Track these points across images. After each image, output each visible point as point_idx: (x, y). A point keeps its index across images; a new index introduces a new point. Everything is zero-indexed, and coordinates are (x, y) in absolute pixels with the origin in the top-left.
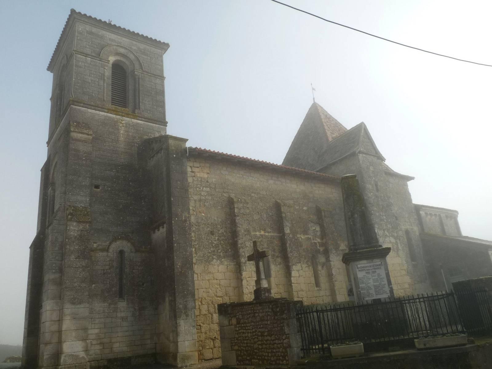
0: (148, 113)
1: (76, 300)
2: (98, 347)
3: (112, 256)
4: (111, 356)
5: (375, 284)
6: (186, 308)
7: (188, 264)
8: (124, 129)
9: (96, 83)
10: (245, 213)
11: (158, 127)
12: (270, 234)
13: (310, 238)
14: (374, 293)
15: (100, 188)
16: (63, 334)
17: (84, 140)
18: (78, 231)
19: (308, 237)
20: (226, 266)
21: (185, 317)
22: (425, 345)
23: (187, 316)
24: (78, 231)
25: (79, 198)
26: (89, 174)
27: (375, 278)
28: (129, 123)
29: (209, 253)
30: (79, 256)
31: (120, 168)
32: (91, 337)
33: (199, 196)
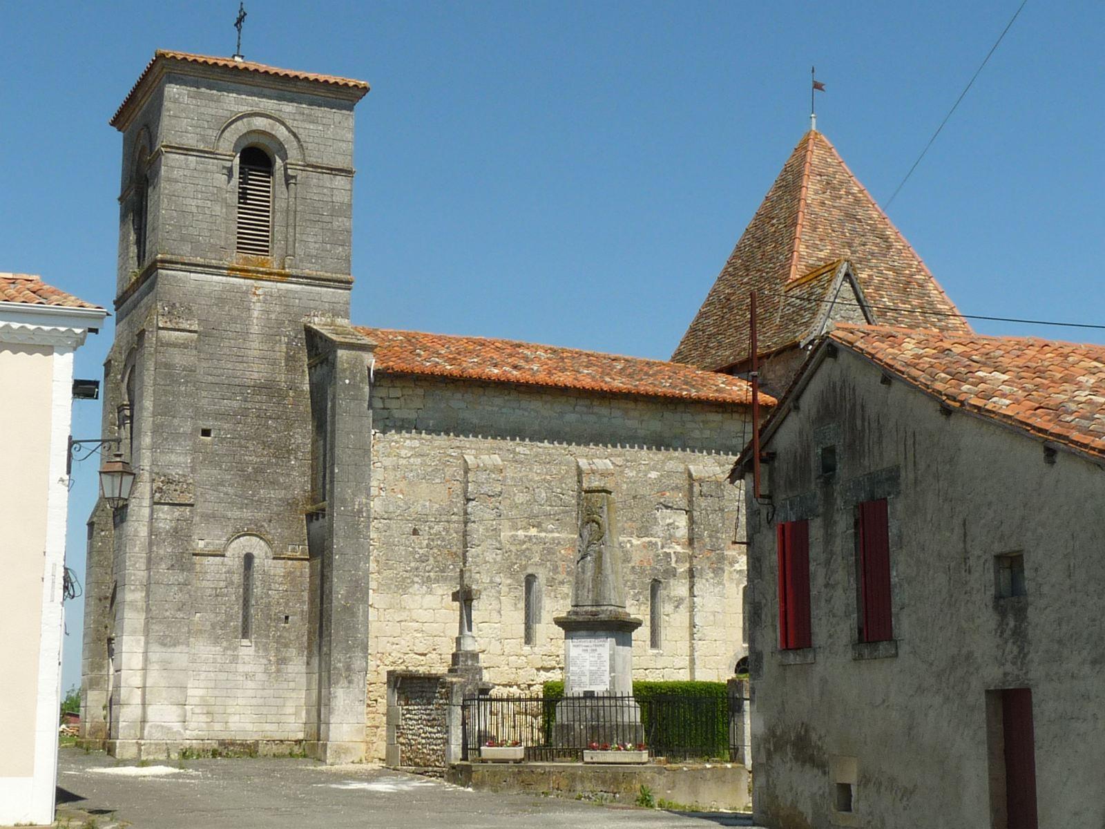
0: (312, 263)
1: (169, 639)
2: (204, 718)
3: (230, 563)
4: (226, 736)
5: (592, 668)
6: (348, 668)
7: (359, 591)
8: (261, 307)
9: (207, 212)
10: (490, 493)
11: (334, 292)
12: (550, 535)
13: (656, 542)
14: (588, 683)
15: (212, 435)
16: (124, 641)
17: (182, 344)
18: (171, 521)
19: (650, 542)
20: (440, 599)
21: (346, 684)
22: (592, 758)
23: (350, 682)
24: (171, 521)
25: (173, 457)
26: (190, 410)
27: (593, 659)
28: (271, 292)
29: (406, 571)
30: (173, 565)
31: (249, 391)
32: (190, 701)
33: (395, 458)
